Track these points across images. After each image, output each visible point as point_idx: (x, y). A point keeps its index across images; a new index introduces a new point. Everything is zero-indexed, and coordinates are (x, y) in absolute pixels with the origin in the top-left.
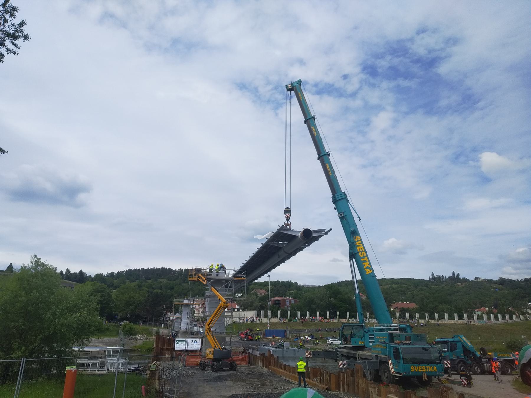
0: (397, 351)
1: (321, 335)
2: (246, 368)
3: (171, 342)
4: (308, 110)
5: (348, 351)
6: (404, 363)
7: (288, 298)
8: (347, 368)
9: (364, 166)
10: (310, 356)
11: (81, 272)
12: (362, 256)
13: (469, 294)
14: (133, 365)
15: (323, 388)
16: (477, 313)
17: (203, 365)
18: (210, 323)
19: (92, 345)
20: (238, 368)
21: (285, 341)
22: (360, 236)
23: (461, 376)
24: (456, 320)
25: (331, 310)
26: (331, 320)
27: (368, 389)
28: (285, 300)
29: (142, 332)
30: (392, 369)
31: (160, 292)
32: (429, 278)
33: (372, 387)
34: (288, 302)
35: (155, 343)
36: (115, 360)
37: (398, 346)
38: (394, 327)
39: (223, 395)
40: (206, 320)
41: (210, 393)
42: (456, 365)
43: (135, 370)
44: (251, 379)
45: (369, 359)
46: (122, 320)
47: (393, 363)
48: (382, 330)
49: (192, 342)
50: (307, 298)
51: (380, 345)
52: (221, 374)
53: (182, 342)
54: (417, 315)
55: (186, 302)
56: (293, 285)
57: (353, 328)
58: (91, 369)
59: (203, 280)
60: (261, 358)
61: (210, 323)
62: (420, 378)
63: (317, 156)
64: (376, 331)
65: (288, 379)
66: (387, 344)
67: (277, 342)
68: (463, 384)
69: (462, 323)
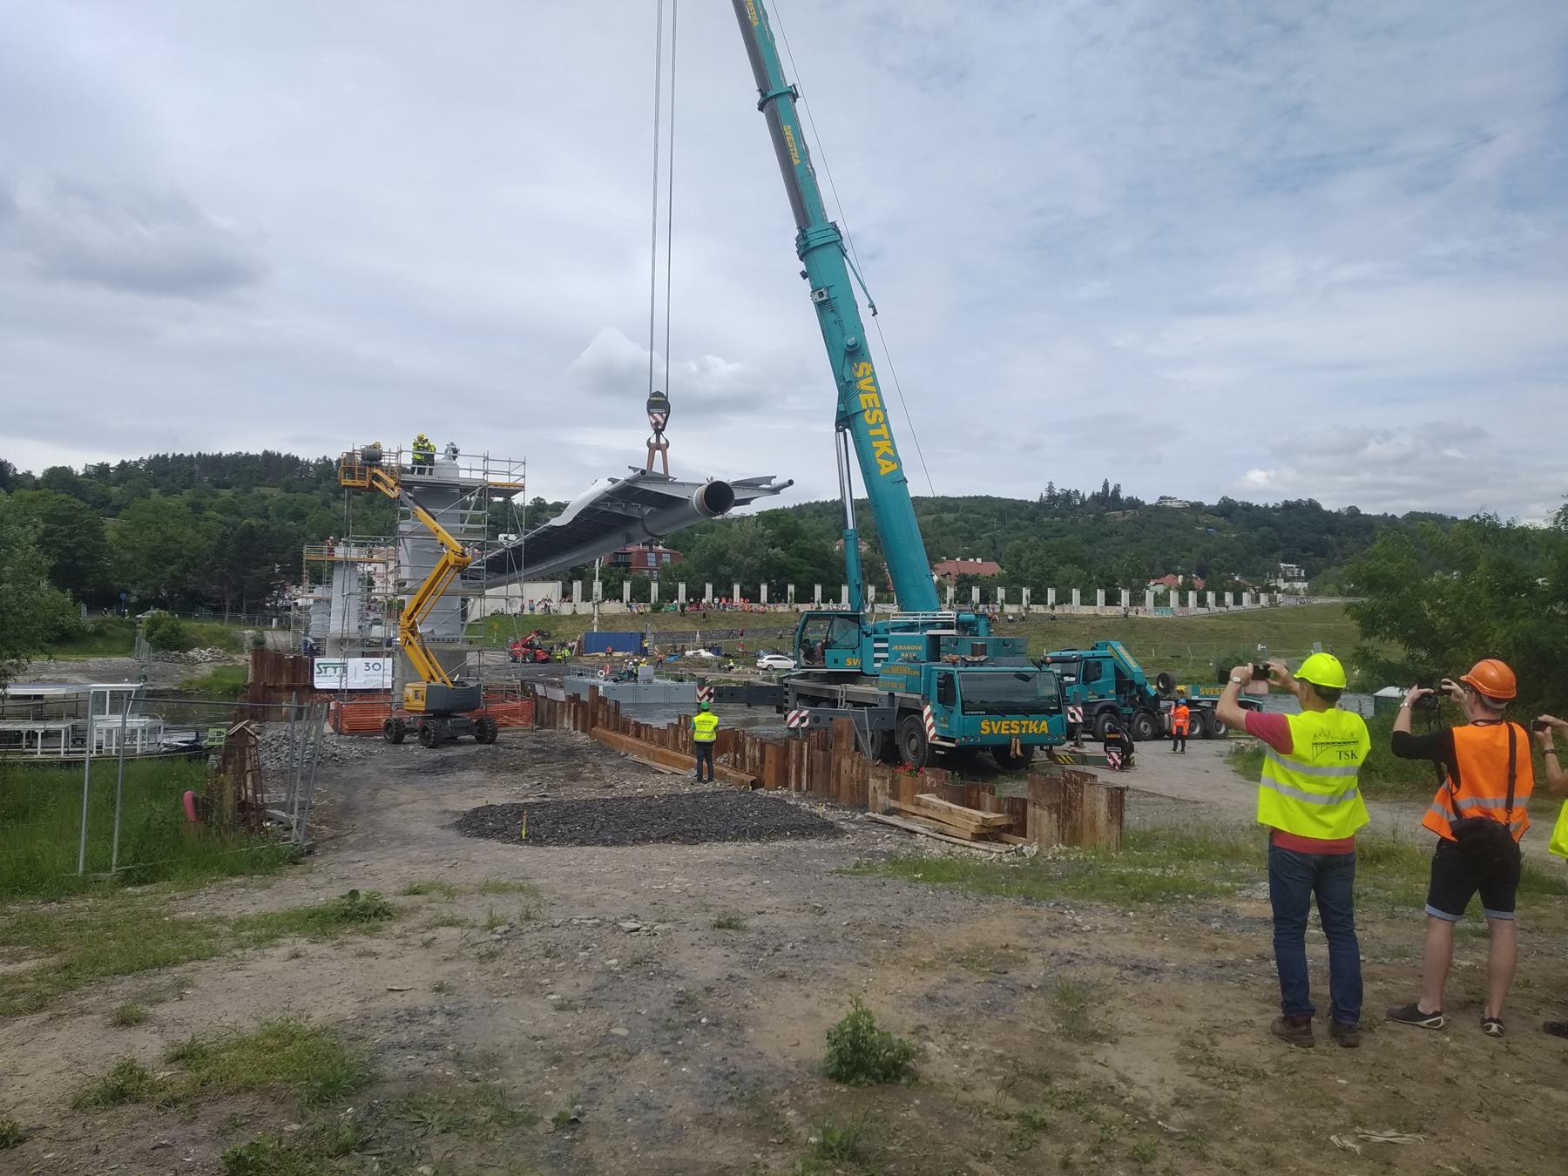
0: (947, 682)
1: (743, 646)
2: (524, 734)
6: (964, 714)
8: (809, 729)
12: (872, 422)
18: (415, 610)
20: (499, 736)
22: (870, 362)
23: (1109, 743)
24: (1100, 608)
26: (772, 605)
27: (865, 784)
29: (209, 640)
30: (930, 728)
35: (250, 672)
36: (115, 721)
37: (952, 669)
42: (1094, 718)
46: (142, 606)
48: (911, 627)
52: (450, 754)
54: (1001, 593)
55: (340, 552)
57: (832, 623)
59: (387, 488)
60: (569, 707)
61: (415, 610)
62: (1001, 750)
63: (758, 97)
64: (894, 630)
67: (618, 665)
68: (1108, 764)
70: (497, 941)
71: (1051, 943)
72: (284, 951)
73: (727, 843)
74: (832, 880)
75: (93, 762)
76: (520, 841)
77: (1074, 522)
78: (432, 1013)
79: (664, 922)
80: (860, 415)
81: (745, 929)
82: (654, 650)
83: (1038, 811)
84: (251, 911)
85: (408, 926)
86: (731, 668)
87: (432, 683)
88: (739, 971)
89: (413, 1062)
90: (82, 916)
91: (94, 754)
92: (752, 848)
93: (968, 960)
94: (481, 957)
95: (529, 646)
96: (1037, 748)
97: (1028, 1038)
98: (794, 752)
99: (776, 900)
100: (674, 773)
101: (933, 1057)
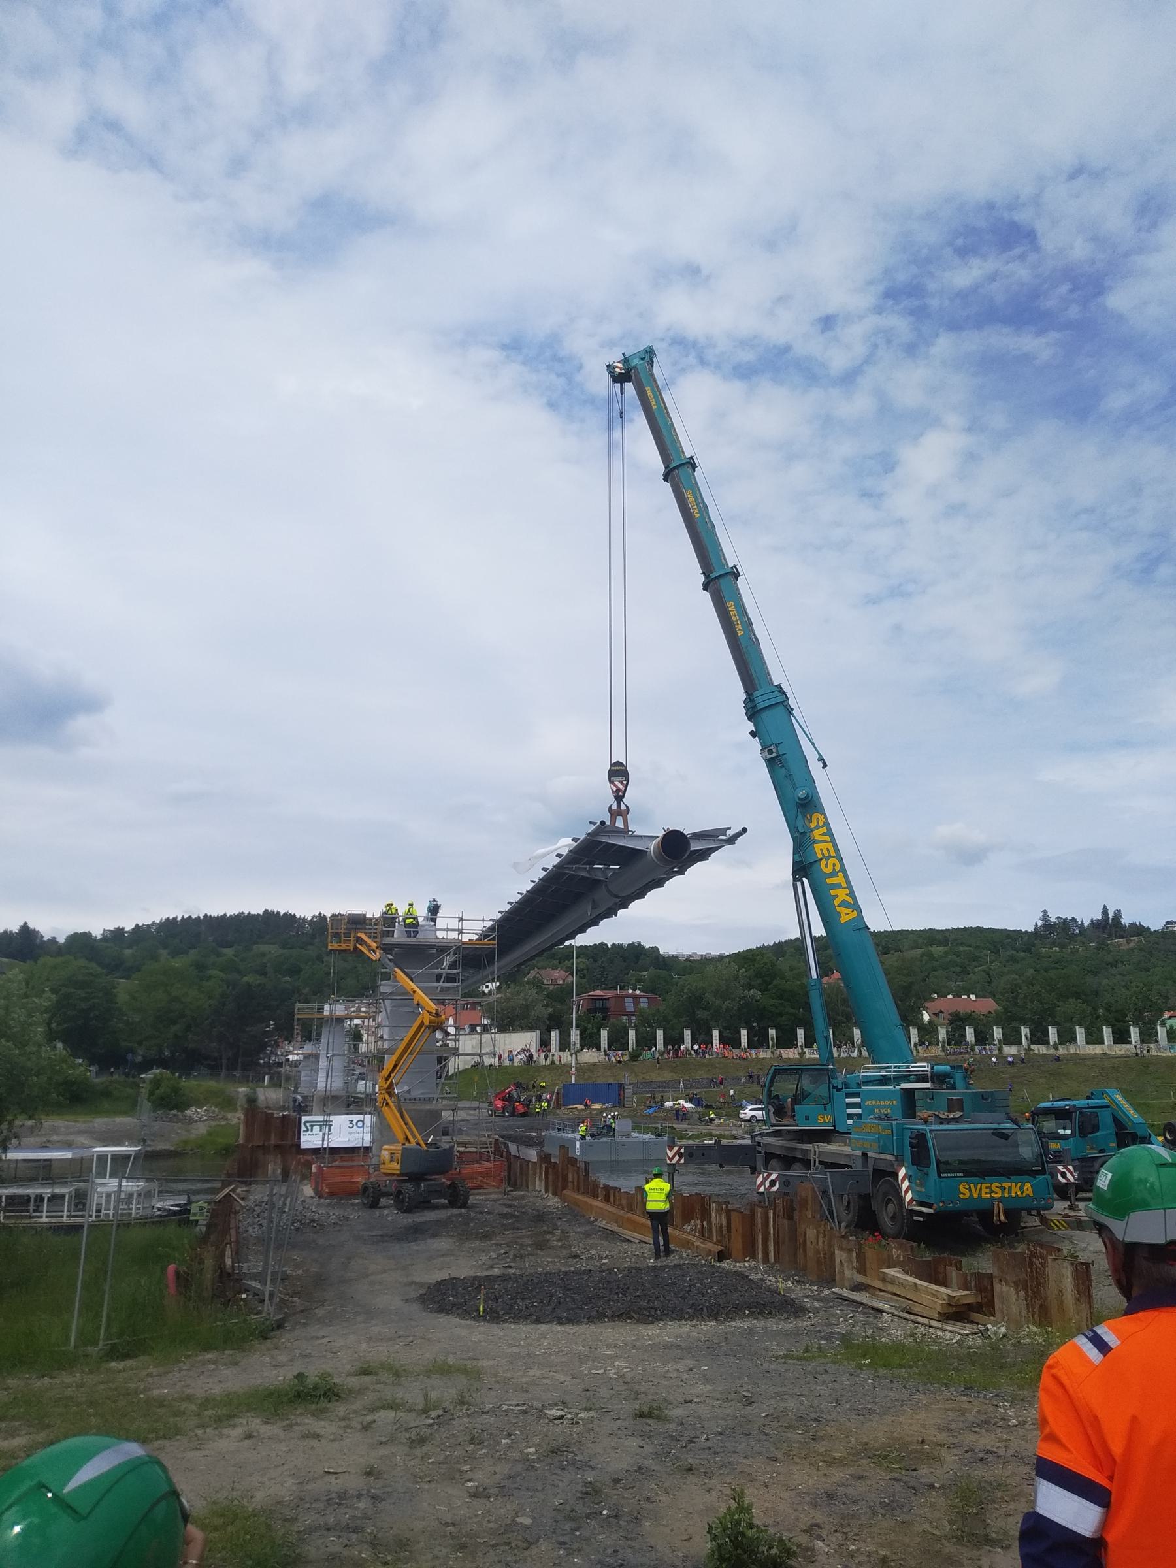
3: (290, 1128)
4: (676, 441)
5: (787, 1144)
6: (939, 1176)
7: (630, 991)
9: (872, 601)
10: (679, 1160)
11: (25, 928)
12: (829, 870)
13: (1147, 970)
14: (172, 1197)
15: (710, 1251)
16: (1169, 1022)
17: (373, 1192)
18: (392, 1071)
19: (58, 1141)
20: (472, 1200)
21: (618, 1115)
22: (823, 813)
24: (1108, 1045)
25: (755, 1024)
26: (753, 1051)
27: (833, 1254)
28: (621, 999)
29: (205, 1099)
30: (906, 1192)
31: (259, 981)
32: (1036, 925)
33: (841, 1248)
34: (629, 1005)
35: (241, 1131)
37: (924, 1127)
38: (918, 1071)
39: (418, 1280)
40: (381, 1060)
41: (383, 1275)
43: (174, 1213)
44: (508, 1230)
45: (844, 1166)
46: (146, 1066)
47: (911, 1176)
48: (884, 1081)
49: (351, 1126)
50: (685, 991)
51: (875, 1124)
52: (423, 1219)
53: (321, 1126)
54: (997, 1033)
56: (645, 954)
57: (800, 1077)
58: (47, 1212)
59: (369, 951)
60: (541, 1168)
61: (392, 1071)
62: (985, 1215)
63: (702, 578)
64: (866, 1083)
65: (613, 1227)
66: (894, 1123)
69: (1124, 1052)
70: (431, 1425)
71: (970, 1438)
72: (239, 1431)
73: (683, 1322)
74: (773, 1366)
75: (92, 1226)
76: (478, 1318)
77: (1074, 952)
78: (359, 1496)
79: (590, 1409)
80: (816, 865)
81: (667, 1420)
82: (633, 1101)
83: (1005, 1288)
84: (217, 1390)
85: (354, 1407)
86: (712, 1120)
87: (407, 1145)
88: (649, 1463)
89: (334, 1544)
90: (69, 1392)
91: (94, 1218)
92: (707, 1328)
93: (880, 1457)
94: (413, 1441)
95: (508, 1099)
96: (1024, 1213)
97: (917, 1540)
98: (759, 1221)
99: (709, 1387)
100: (642, 1241)
101: (820, 1557)
